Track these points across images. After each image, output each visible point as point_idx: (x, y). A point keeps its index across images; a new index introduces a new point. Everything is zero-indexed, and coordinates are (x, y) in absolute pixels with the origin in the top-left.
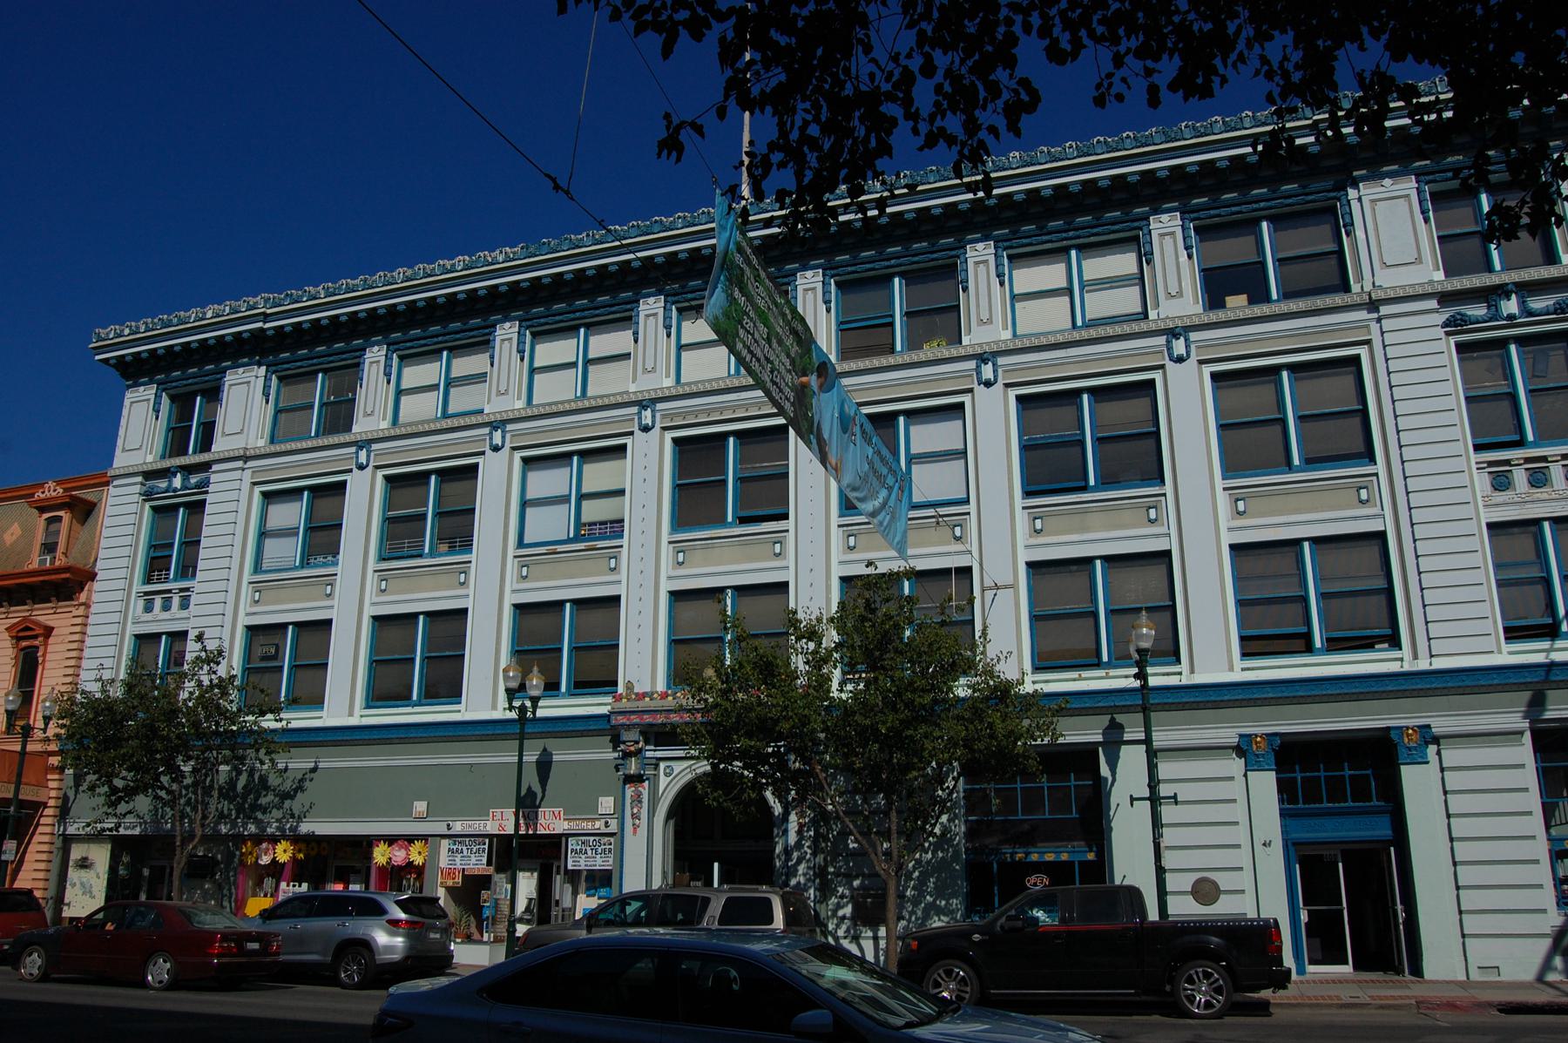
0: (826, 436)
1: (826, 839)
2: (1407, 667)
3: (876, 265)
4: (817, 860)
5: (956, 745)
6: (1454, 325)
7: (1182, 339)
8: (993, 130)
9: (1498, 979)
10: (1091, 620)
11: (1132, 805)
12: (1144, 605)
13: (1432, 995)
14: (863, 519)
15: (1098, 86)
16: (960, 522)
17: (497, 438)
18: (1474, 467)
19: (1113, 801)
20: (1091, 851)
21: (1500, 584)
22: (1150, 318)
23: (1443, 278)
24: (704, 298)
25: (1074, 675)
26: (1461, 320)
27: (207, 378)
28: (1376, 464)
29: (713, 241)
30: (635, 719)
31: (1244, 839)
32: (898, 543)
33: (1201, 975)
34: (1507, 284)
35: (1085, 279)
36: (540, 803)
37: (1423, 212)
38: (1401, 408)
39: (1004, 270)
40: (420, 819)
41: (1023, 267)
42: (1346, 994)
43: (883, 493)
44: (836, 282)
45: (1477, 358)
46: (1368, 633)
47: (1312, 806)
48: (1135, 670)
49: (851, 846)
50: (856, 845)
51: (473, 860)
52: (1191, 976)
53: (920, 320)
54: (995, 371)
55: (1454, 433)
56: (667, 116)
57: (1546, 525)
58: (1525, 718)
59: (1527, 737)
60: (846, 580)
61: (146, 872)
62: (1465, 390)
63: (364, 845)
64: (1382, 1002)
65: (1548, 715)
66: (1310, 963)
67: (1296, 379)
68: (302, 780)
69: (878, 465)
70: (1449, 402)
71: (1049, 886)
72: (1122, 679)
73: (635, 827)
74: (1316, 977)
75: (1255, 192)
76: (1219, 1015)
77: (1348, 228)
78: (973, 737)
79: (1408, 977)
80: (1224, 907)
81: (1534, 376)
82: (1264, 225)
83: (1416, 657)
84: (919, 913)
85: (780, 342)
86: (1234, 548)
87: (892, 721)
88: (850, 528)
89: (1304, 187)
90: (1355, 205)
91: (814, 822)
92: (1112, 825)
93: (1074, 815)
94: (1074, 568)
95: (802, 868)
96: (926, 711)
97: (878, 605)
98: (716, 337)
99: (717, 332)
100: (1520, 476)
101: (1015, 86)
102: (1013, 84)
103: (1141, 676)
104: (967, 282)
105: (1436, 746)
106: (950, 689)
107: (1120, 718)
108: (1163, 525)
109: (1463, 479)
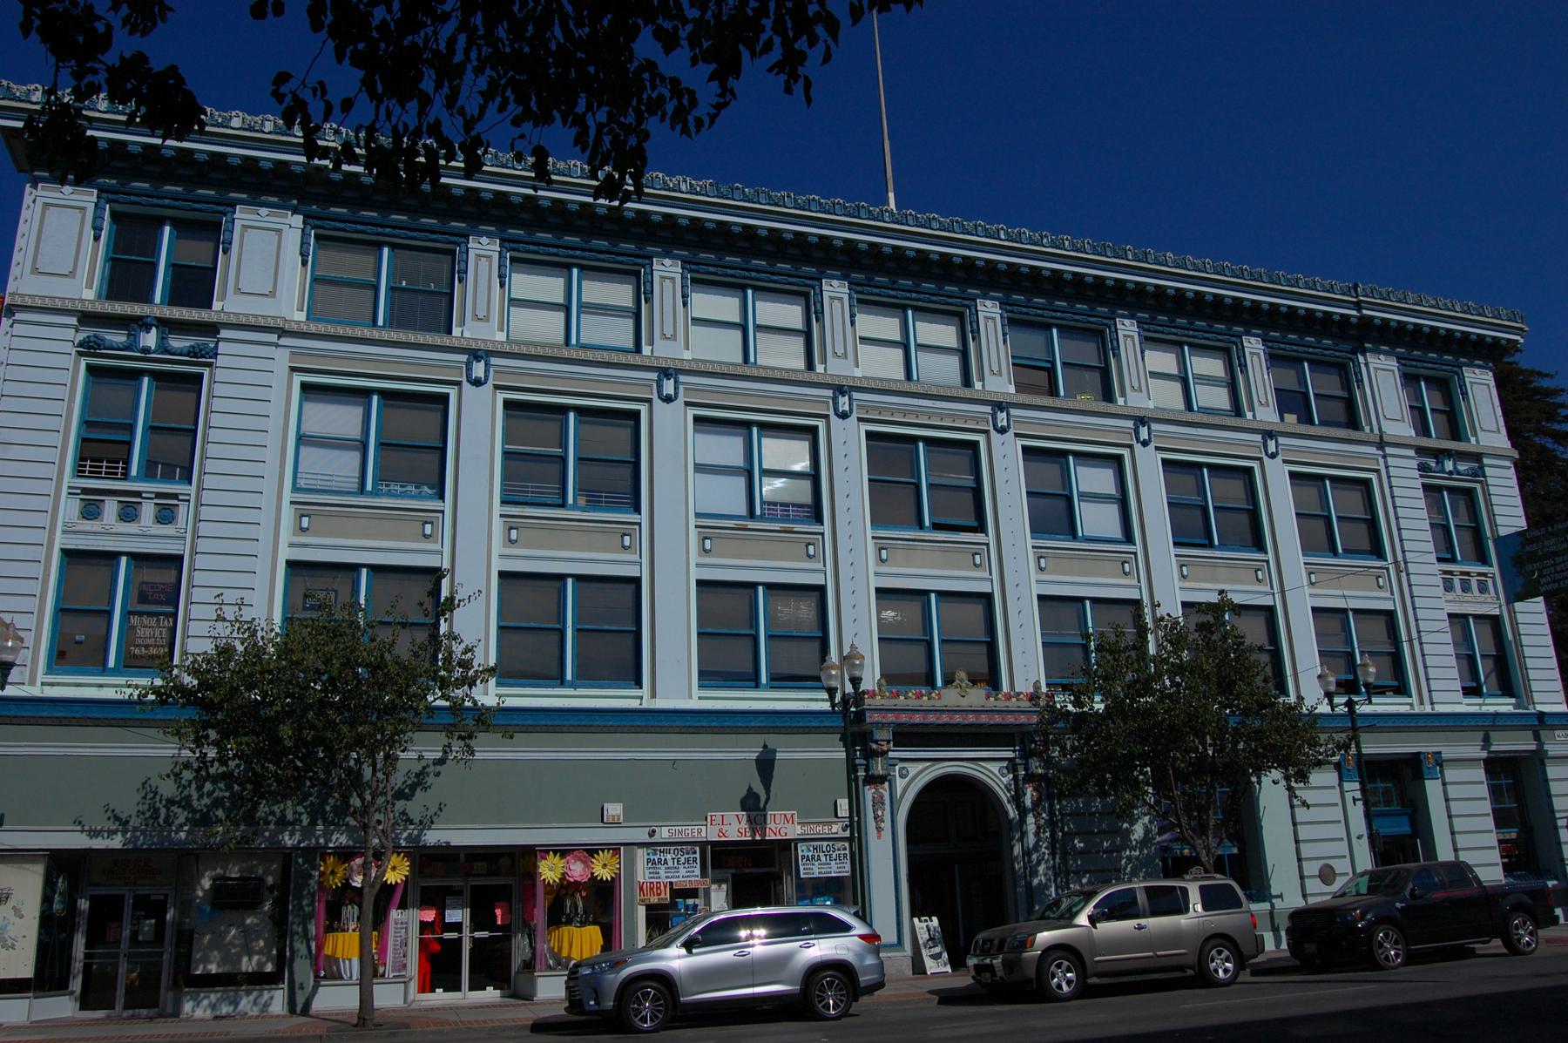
2: (645, 705)
6: (88, 348)
7: (483, 362)
16: (431, 520)
17: (669, 386)
18: (65, 490)
23: (304, 320)
27: (197, 206)
30: (891, 718)
36: (765, 806)
40: (616, 824)
44: (316, 235)
50: (1082, 845)
51: (682, 871)
57: (933, 596)
58: (1482, 749)
61: (84, 904)
63: (530, 854)
68: (422, 774)
73: (879, 829)
83: (1422, 703)
89: (1336, 345)
95: (1041, 869)
104: (231, 243)
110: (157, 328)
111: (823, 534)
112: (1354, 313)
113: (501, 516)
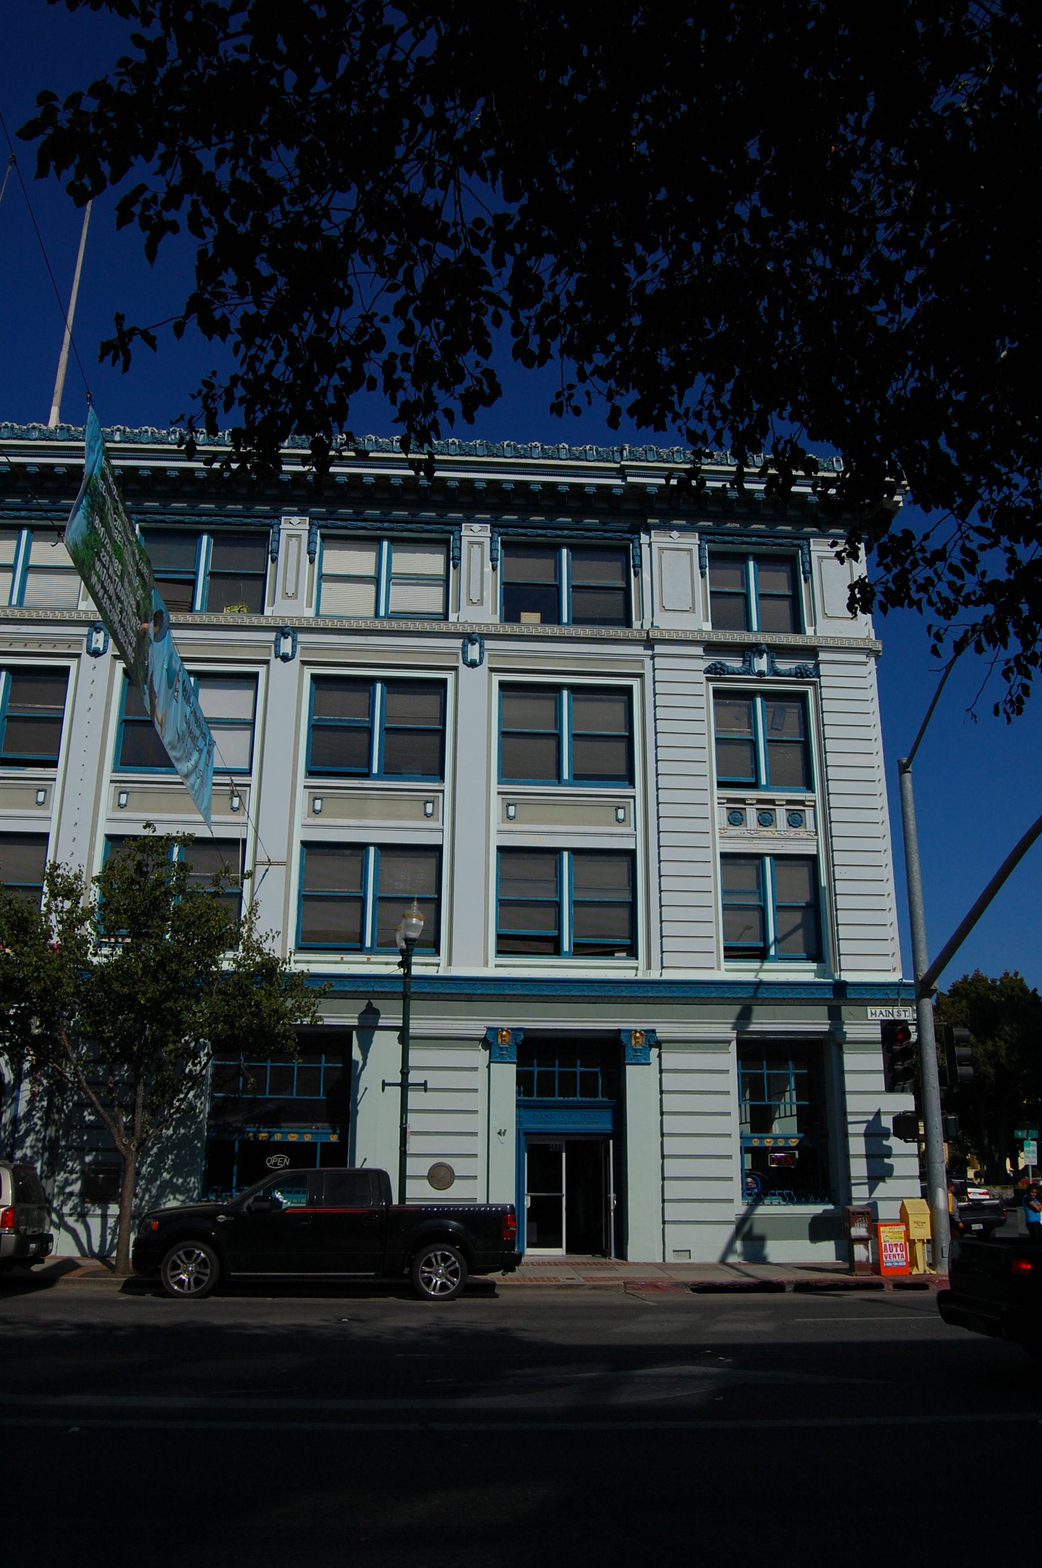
0: (156, 689)
1: (60, 1111)
2: (641, 976)
3: (186, 518)
4: (48, 1132)
5: (216, 1020)
6: (715, 672)
7: (290, 639)
8: (449, 414)
9: (689, 1261)
10: (358, 905)
11: (383, 1090)
12: (416, 896)
13: (642, 1276)
14: (177, 778)
15: (558, 395)
16: (45, 788)
17: (286, 646)
18: (716, 801)
19: (362, 1084)
20: (334, 1133)
21: (725, 907)
22: (450, 620)
23: (710, 629)
24: (66, 519)
25: (336, 957)
26: (721, 669)
28: (634, 788)
29: (82, 461)
31: (482, 1130)
32: (205, 809)
33: (439, 1258)
34: (761, 644)
35: (393, 571)
37: (701, 568)
38: (662, 740)
39: (315, 547)
41: (336, 549)
42: (563, 1275)
43: (195, 756)
45: (729, 705)
46: (611, 941)
47: (545, 1099)
48: (399, 959)
49: (87, 1118)
50: (92, 1118)
52: (430, 1258)
53: (221, 582)
54: (294, 647)
55: (703, 769)
56: (119, 319)
57: (768, 860)
59: (734, 1044)
60: (112, 839)
62: (716, 731)
64: (595, 1283)
65: (753, 1028)
66: (528, 1247)
67: (574, 699)
69: (193, 727)
70: (702, 741)
71: (290, 1167)
72: (387, 965)
74: (534, 1259)
75: (506, 517)
76: (451, 1298)
77: (637, 569)
78: (235, 1013)
79: (614, 1259)
80: (458, 1193)
81: (772, 728)
82: (565, 551)
83: (649, 967)
84: (154, 1191)
85: (130, 583)
86: (501, 849)
87: (153, 992)
88: (123, 785)
89: (604, 524)
90: (645, 549)
91: (49, 1092)
92: (359, 1108)
93: (322, 1097)
94: (348, 852)
95: (29, 1141)
96: (186, 983)
97: (150, 869)
98: (73, 565)
99: (75, 560)
100: (751, 814)
101: (480, 376)
102: (477, 372)
103: (405, 964)
105: (657, 1050)
106: (215, 963)
107: (377, 1004)
108: (438, 820)
109: (705, 811)
110: (767, 653)
111: (634, 797)
112: (618, 482)
113: (499, 793)
